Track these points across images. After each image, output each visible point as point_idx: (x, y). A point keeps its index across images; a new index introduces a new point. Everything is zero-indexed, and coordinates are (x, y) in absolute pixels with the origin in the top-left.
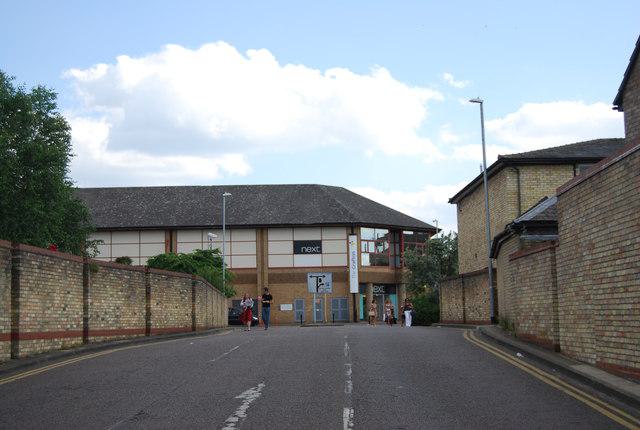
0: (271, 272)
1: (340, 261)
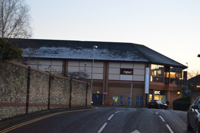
0: (109, 82)
1: (141, 79)
